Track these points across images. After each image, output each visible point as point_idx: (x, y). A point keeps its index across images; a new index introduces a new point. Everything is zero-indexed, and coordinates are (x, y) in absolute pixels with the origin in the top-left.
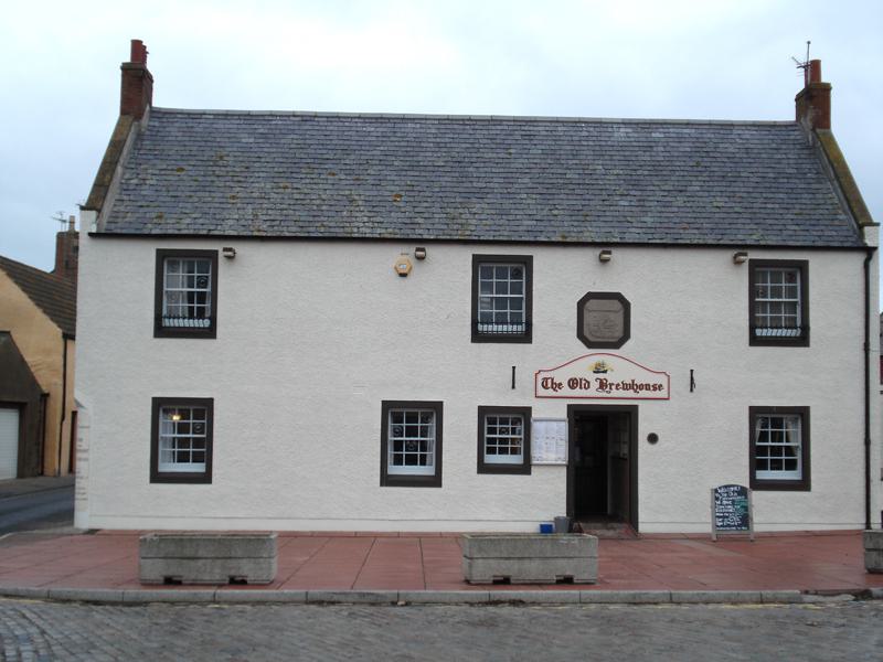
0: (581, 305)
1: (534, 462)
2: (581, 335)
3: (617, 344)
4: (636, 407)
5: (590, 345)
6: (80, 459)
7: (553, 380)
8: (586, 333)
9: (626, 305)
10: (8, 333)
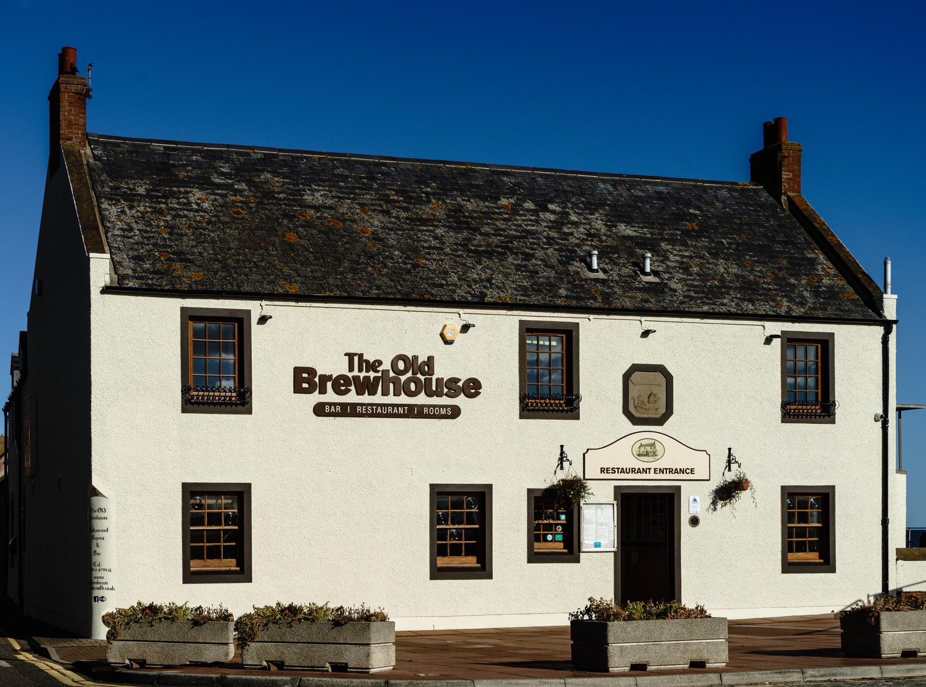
0: (627, 377)
1: (584, 549)
2: (626, 411)
3: (661, 421)
4: (679, 488)
5: (635, 421)
6: (97, 518)
7: (361, 356)
8: (631, 409)
9: (669, 378)
10: (76, 50)
